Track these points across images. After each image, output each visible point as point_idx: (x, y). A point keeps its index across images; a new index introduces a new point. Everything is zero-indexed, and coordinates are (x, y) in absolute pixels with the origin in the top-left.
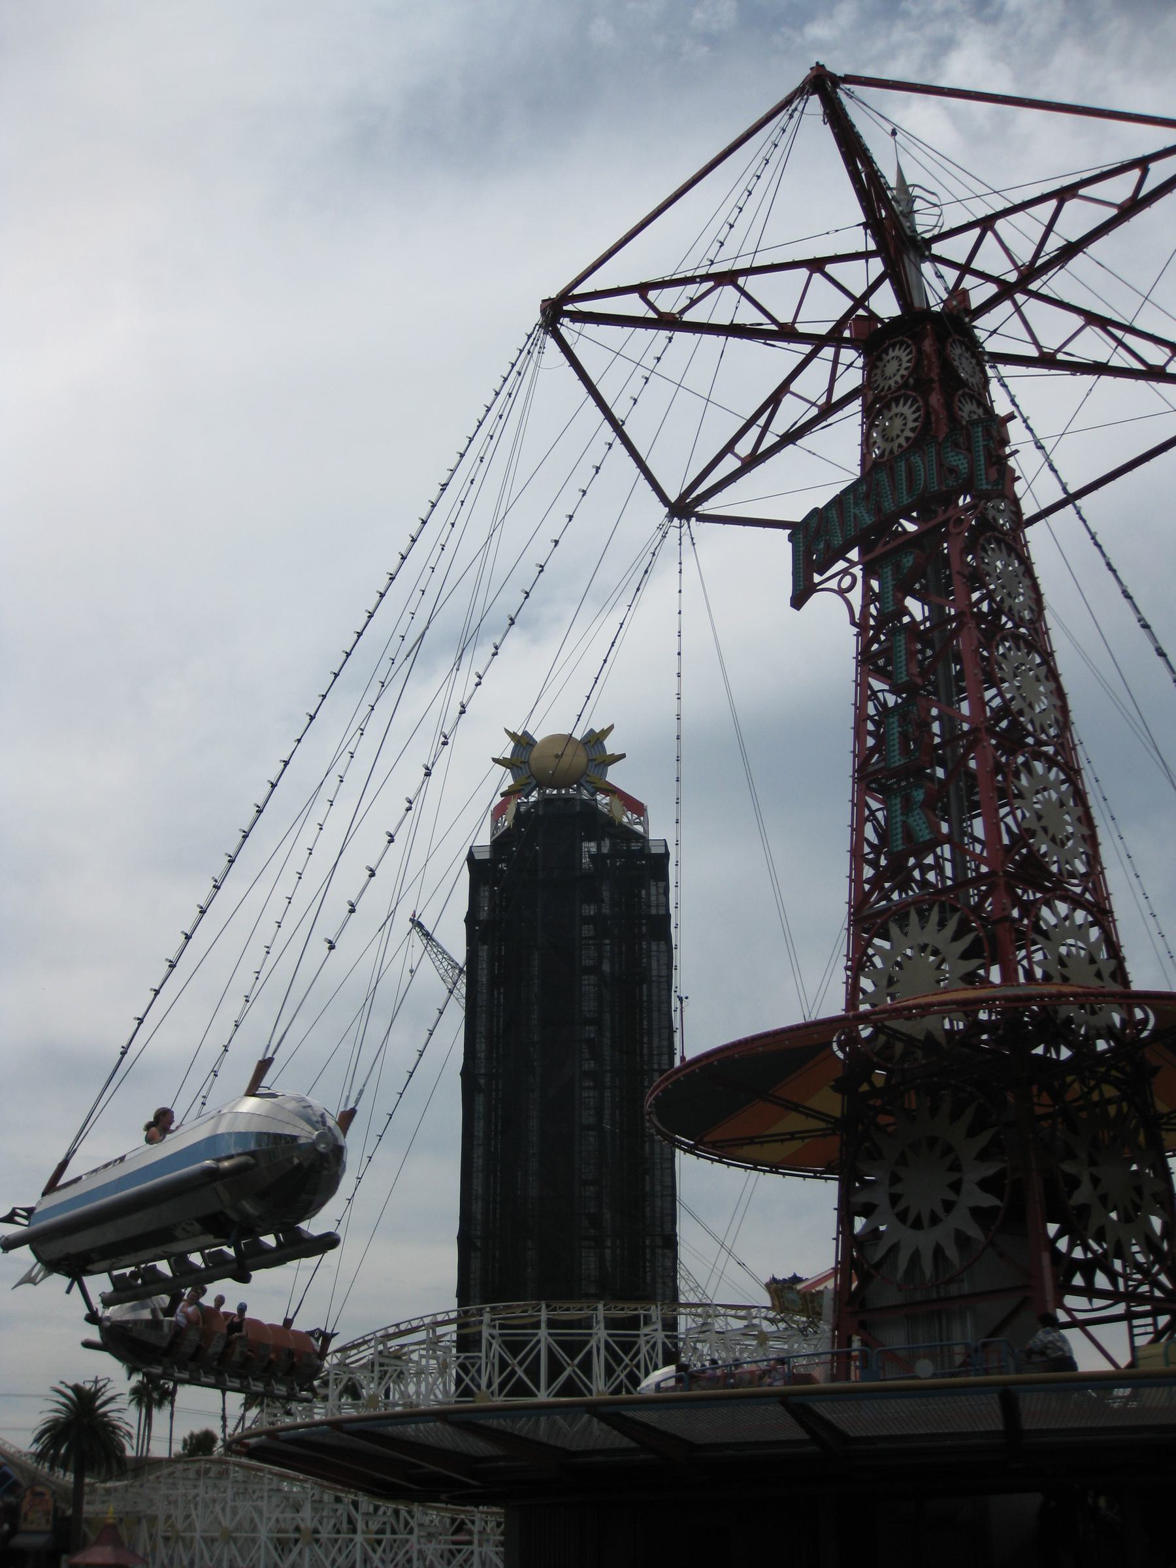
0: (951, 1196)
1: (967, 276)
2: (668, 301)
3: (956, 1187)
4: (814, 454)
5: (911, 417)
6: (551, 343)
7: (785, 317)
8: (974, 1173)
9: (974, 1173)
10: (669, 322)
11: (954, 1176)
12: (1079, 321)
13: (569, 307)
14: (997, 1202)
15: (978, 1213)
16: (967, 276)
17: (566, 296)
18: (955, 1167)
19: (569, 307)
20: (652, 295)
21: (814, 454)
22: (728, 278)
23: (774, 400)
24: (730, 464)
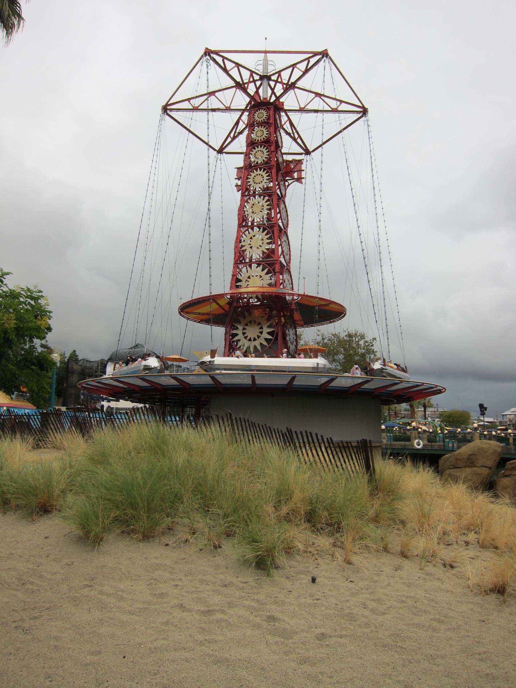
0: (260, 335)
1: (276, 79)
2: (196, 102)
3: (261, 333)
4: (325, 70)
5: (265, 135)
6: (167, 117)
7: (228, 105)
8: (266, 330)
9: (266, 330)
10: (196, 109)
11: (261, 330)
12: (314, 95)
13: (168, 108)
14: (271, 337)
15: (266, 340)
16: (276, 79)
17: (167, 105)
18: (261, 328)
19: (168, 108)
20: (192, 101)
21: (325, 70)
22: (213, 93)
23: (237, 123)
24: (229, 139)
